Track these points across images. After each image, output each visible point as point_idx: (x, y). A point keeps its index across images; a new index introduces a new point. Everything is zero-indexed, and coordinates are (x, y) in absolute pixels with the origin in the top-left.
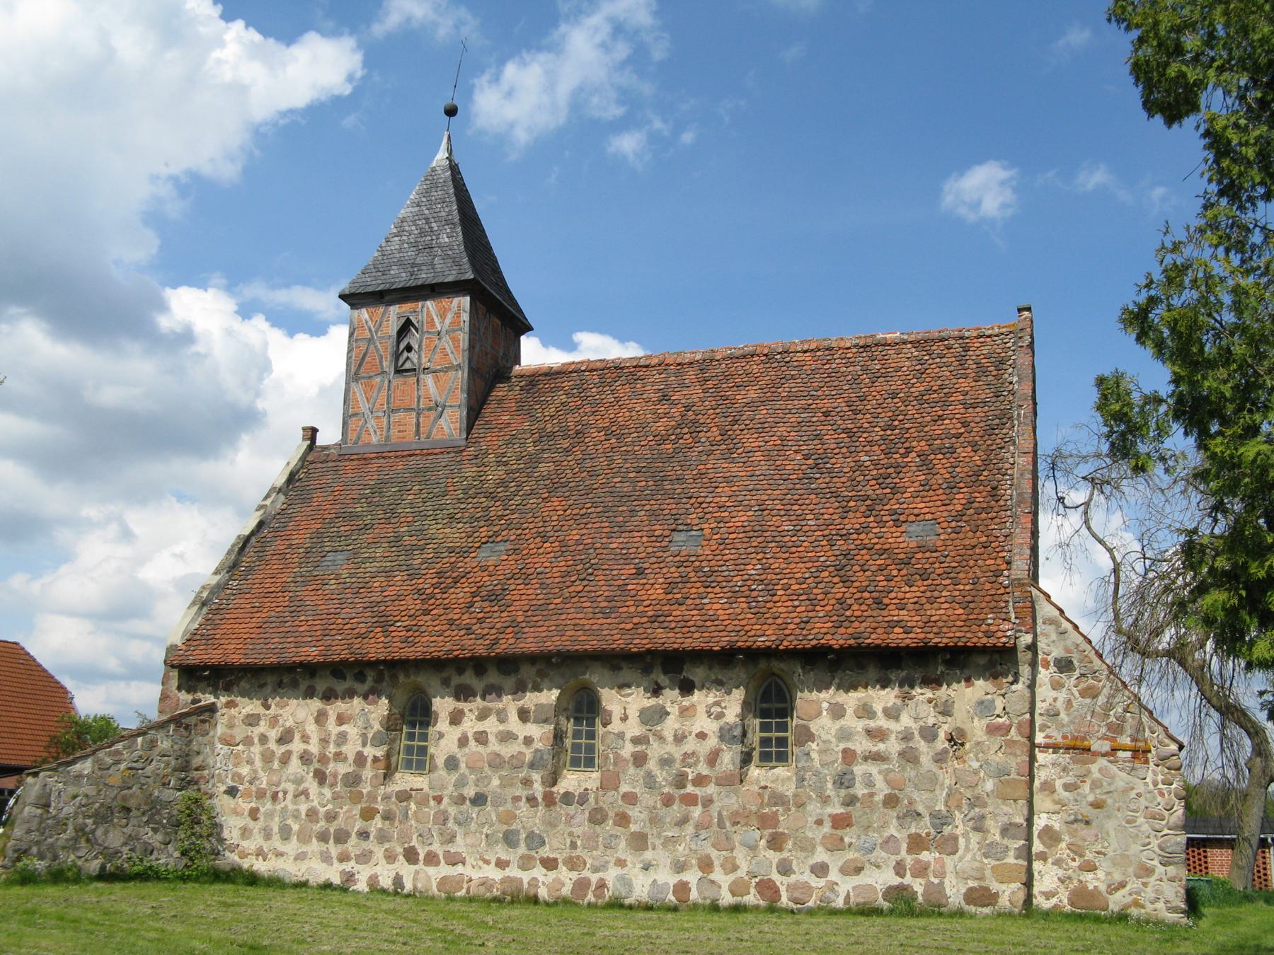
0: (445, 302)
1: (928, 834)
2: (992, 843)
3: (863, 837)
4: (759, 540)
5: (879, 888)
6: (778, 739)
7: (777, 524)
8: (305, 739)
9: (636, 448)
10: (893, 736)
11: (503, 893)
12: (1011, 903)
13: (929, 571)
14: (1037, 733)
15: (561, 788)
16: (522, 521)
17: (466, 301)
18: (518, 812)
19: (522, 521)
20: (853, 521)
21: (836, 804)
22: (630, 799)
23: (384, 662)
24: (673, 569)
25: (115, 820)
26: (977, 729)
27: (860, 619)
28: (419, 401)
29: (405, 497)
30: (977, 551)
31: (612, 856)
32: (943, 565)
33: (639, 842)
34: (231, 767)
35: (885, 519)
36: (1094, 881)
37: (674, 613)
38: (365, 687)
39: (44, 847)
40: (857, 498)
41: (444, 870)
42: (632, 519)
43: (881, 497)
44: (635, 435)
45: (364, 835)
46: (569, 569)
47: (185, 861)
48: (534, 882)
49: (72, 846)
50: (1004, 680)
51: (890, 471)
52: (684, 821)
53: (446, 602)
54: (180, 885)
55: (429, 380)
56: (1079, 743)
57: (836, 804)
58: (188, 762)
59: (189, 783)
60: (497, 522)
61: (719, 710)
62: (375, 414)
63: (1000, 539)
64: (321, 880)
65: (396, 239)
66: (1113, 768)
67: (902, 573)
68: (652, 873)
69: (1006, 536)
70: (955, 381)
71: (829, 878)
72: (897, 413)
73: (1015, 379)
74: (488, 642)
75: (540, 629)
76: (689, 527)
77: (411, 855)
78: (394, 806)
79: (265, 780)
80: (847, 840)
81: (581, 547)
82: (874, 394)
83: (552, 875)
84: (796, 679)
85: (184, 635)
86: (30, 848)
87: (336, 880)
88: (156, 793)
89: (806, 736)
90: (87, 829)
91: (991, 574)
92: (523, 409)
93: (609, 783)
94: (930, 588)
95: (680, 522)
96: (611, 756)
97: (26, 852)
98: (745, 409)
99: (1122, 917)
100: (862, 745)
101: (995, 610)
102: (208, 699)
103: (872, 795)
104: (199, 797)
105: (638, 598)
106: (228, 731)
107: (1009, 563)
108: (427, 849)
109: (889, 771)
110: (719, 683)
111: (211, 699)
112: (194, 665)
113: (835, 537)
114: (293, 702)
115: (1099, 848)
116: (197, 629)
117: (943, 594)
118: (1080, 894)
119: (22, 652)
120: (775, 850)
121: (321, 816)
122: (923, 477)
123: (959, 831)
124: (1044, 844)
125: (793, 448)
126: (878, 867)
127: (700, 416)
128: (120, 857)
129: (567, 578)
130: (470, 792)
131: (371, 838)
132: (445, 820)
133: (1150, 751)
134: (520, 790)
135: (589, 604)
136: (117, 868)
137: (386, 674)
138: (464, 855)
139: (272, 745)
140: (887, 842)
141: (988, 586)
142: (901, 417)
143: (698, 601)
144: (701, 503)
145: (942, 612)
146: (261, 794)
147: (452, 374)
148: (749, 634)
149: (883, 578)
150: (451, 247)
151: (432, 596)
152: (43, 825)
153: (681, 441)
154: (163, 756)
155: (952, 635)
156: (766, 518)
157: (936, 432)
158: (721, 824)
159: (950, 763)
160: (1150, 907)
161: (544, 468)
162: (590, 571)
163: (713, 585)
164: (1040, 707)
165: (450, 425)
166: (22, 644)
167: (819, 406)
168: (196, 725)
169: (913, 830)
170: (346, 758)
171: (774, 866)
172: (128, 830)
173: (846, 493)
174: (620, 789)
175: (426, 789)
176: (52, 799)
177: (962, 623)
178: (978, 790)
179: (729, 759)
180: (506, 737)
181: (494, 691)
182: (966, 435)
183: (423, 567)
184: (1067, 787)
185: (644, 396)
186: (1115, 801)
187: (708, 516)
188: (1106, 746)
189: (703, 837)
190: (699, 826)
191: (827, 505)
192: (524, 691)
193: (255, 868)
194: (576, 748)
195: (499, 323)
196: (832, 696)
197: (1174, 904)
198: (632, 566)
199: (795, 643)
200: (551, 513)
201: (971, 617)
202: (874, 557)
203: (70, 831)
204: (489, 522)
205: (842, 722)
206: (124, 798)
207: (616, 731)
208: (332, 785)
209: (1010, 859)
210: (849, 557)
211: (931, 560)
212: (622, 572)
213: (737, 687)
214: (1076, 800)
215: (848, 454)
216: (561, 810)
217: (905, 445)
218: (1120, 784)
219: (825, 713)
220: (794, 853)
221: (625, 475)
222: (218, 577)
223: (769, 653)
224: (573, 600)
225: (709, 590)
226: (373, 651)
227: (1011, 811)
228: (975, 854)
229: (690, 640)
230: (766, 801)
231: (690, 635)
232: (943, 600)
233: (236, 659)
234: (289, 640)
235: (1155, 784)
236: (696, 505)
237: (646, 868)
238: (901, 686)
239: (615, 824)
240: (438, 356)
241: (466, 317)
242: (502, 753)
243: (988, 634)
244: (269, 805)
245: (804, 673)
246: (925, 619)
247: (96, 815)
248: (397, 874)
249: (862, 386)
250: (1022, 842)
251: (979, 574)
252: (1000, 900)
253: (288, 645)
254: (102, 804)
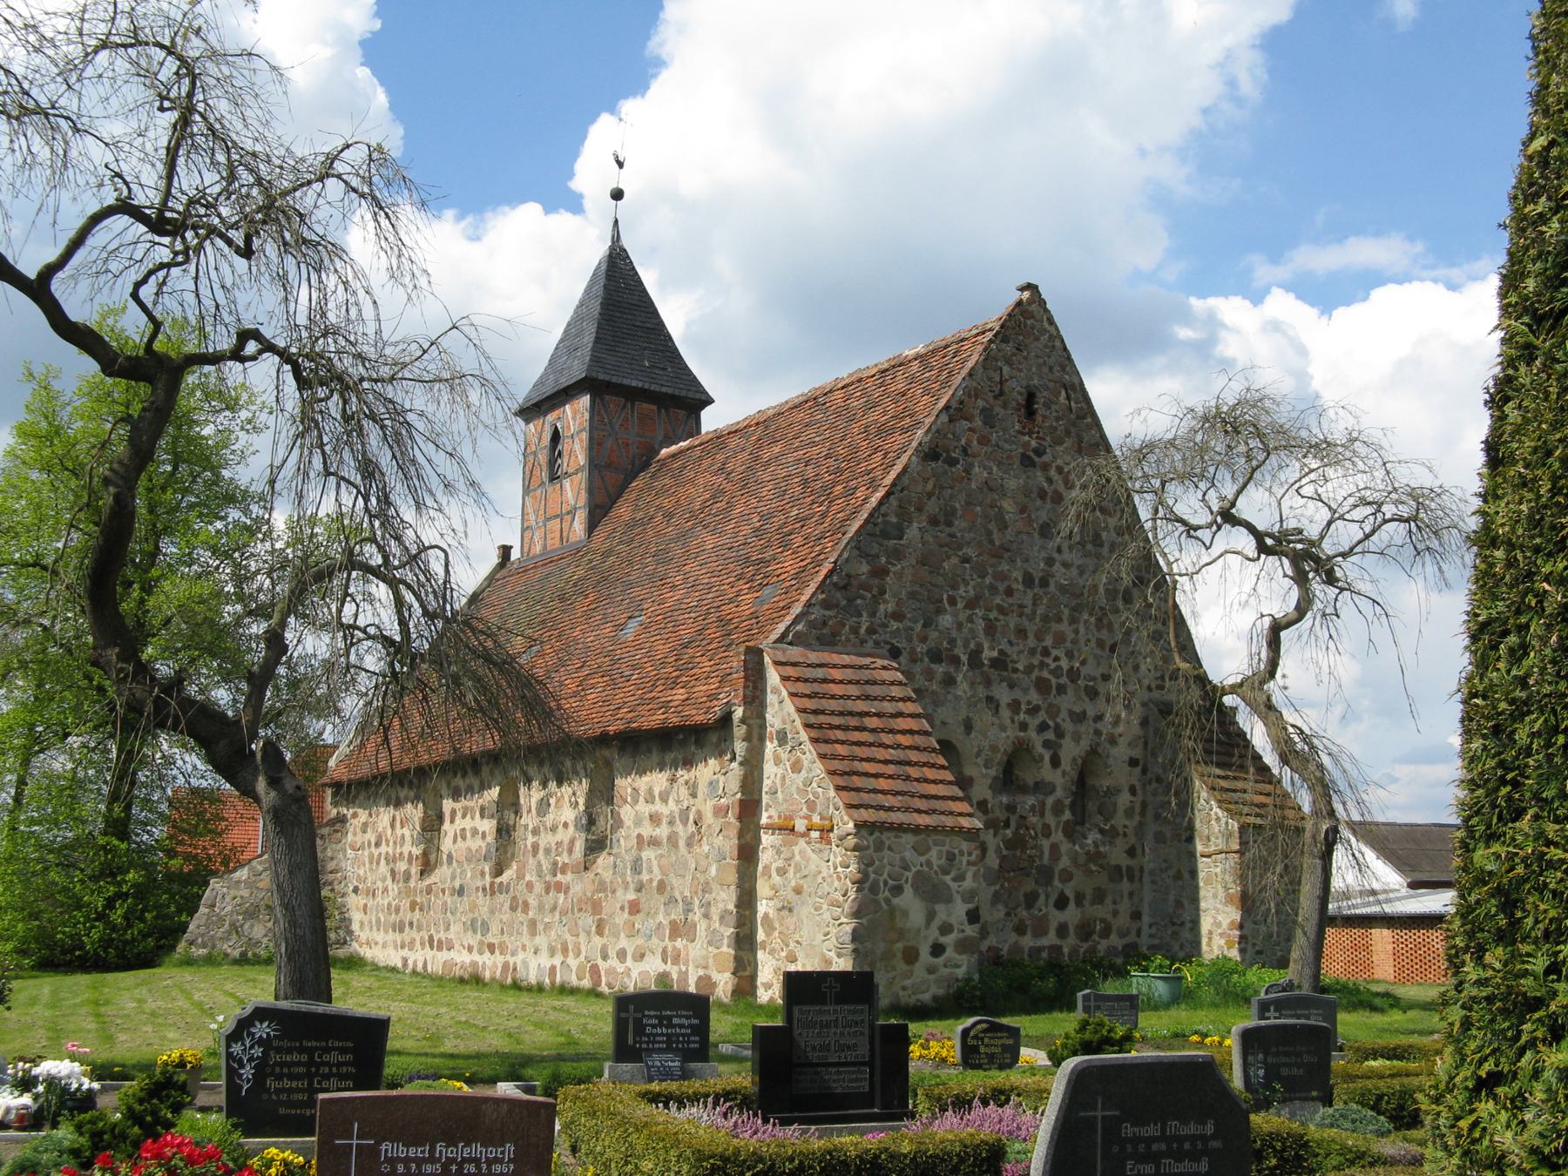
165: (579, 527)
218: (812, 867)
247: (245, 913)
250: (732, 930)
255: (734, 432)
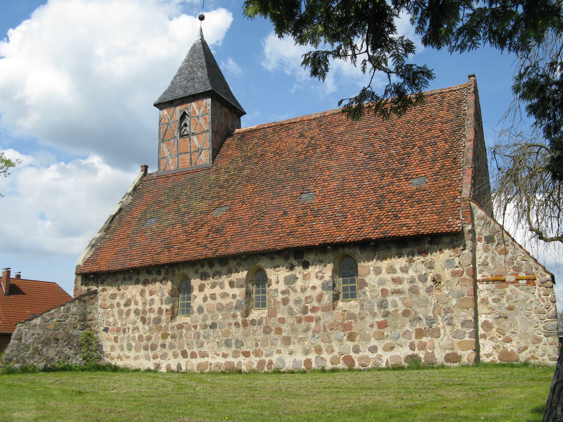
0: (200, 102)
1: (425, 328)
2: (457, 331)
3: (393, 332)
4: (341, 193)
5: (402, 356)
6: (351, 287)
7: (350, 186)
8: (136, 303)
9: (287, 159)
10: (405, 281)
11: (226, 369)
12: (468, 361)
13: (421, 200)
14: (478, 274)
15: (250, 318)
16: (234, 196)
17: (209, 101)
18: (231, 330)
19: (234, 196)
20: (386, 181)
21: (379, 316)
22: (282, 320)
23: (167, 264)
24: (300, 211)
25: (52, 345)
26: (446, 274)
27: (386, 225)
28: (191, 148)
29: (183, 191)
30: (445, 188)
31: (275, 348)
32: (428, 196)
33: (287, 341)
34: (105, 319)
35: (401, 178)
36: (510, 347)
37: (299, 230)
38: (161, 277)
39: (19, 358)
40: (388, 170)
41: (199, 360)
42: (283, 190)
43: (400, 168)
44: (288, 153)
45: (163, 346)
46: (253, 215)
47: (84, 362)
48: (240, 363)
49: (32, 356)
50: (459, 249)
51: (405, 156)
52: (307, 330)
53: (197, 235)
54: (81, 372)
55: (195, 138)
56: (499, 278)
57: (379, 316)
58: (85, 317)
59: (86, 326)
60: (223, 198)
61: (321, 274)
62: (172, 156)
63: (457, 182)
64: (146, 368)
65: (179, 77)
66: (517, 289)
67: (408, 202)
68: (293, 356)
69: (460, 180)
70: (437, 112)
71: (378, 353)
72: (409, 130)
73: (466, 108)
74: (213, 251)
75: (237, 243)
76: (309, 191)
77: (184, 354)
78: (176, 332)
79: (120, 323)
80: (385, 334)
81: (259, 205)
82: (399, 123)
83: (248, 359)
84: (357, 257)
85: (83, 261)
86: (13, 358)
87: (152, 368)
88: (71, 332)
89: (364, 284)
90: (39, 349)
91: (452, 198)
92: (238, 147)
93: (272, 314)
94: (421, 208)
95: (305, 189)
96: (272, 301)
97: (10, 360)
98: (339, 136)
99: (526, 364)
100: (390, 286)
101: (453, 215)
102: (94, 288)
103: (396, 311)
104: (91, 333)
105: (283, 225)
106: (103, 302)
107: (461, 192)
108: (191, 350)
109: (404, 298)
110: (321, 262)
111: (95, 288)
112: (86, 273)
113: (377, 189)
114: (130, 287)
115: (512, 330)
116: (90, 257)
117: (428, 210)
118: (504, 354)
119: (57, 287)
120: (351, 341)
121: (144, 338)
122: (421, 157)
123: (440, 326)
124: (484, 330)
125: (360, 151)
126: (402, 346)
127: (317, 141)
128: (54, 361)
129: (252, 219)
130: (209, 322)
131: (167, 347)
132: (199, 336)
133: (536, 279)
134: (231, 320)
135: (260, 230)
136: (52, 366)
137: (170, 270)
138: (208, 352)
139: (122, 307)
140: (405, 334)
141: (450, 204)
142: (411, 132)
143: (310, 224)
144: (315, 180)
145: (427, 218)
146: (118, 330)
147: (204, 135)
148: (333, 236)
149: (399, 205)
150: (202, 78)
151: (191, 233)
152: (19, 348)
153: (308, 154)
154: (74, 315)
155: (431, 228)
156: (345, 184)
157: (428, 136)
158: (325, 330)
159: (434, 292)
160: (540, 359)
161: (245, 172)
162: (262, 215)
163: (318, 216)
164: (478, 261)
165: (205, 158)
166: (57, 283)
167: (373, 131)
168: (88, 300)
169: (418, 327)
170: (154, 311)
171: (351, 349)
172: (58, 349)
173: (384, 168)
174: (277, 316)
175: (190, 322)
176: (23, 336)
177: (436, 222)
178: (449, 305)
179: (327, 298)
180: (224, 295)
181: (218, 274)
182: (442, 136)
183: (189, 221)
184: (494, 301)
185: (293, 136)
186: (520, 306)
187: (318, 185)
188: (513, 279)
189: (316, 337)
190: (314, 332)
191: (374, 175)
192: (231, 273)
193: (117, 364)
194: (258, 298)
195: (228, 111)
196: (375, 264)
197: (553, 356)
198: (282, 211)
199: (355, 238)
200: (247, 191)
201: (441, 219)
202: (395, 196)
203: (31, 350)
204: (219, 198)
205: (380, 276)
206: (56, 334)
207: (274, 289)
208: (149, 324)
209: (467, 338)
210: (383, 197)
211: (422, 195)
212: (277, 214)
213: (329, 263)
214: (499, 307)
215: (385, 151)
216: (251, 328)
217: (413, 144)
218: (521, 297)
219: (372, 272)
220: (360, 342)
221: (281, 171)
222: (100, 234)
223: (342, 245)
224: (253, 229)
225: (316, 218)
226: (162, 259)
227: (466, 314)
228: (449, 337)
229: (305, 242)
230: (345, 317)
231: (305, 239)
232: (427, 212)
233: (104, 269)
234: (127, 258)
235: (540, 296)
236: (313, 181)
237: (291, 353)
238: (408, 256)
239: (276, 333)
240: (198, 127)
241: (209, 108)
242: (223, 303)
243: (448, 226)
244: (122, 335)
245: (361, 254)
246: (418, 222)
247: (43, 342)
248: (179, 363)
249: (393, 120)
250: (472, 329)
251: (446, 199)
252: (462, 359)
253: (127, 261)
254: (46, 338)
255: (251, 131)
